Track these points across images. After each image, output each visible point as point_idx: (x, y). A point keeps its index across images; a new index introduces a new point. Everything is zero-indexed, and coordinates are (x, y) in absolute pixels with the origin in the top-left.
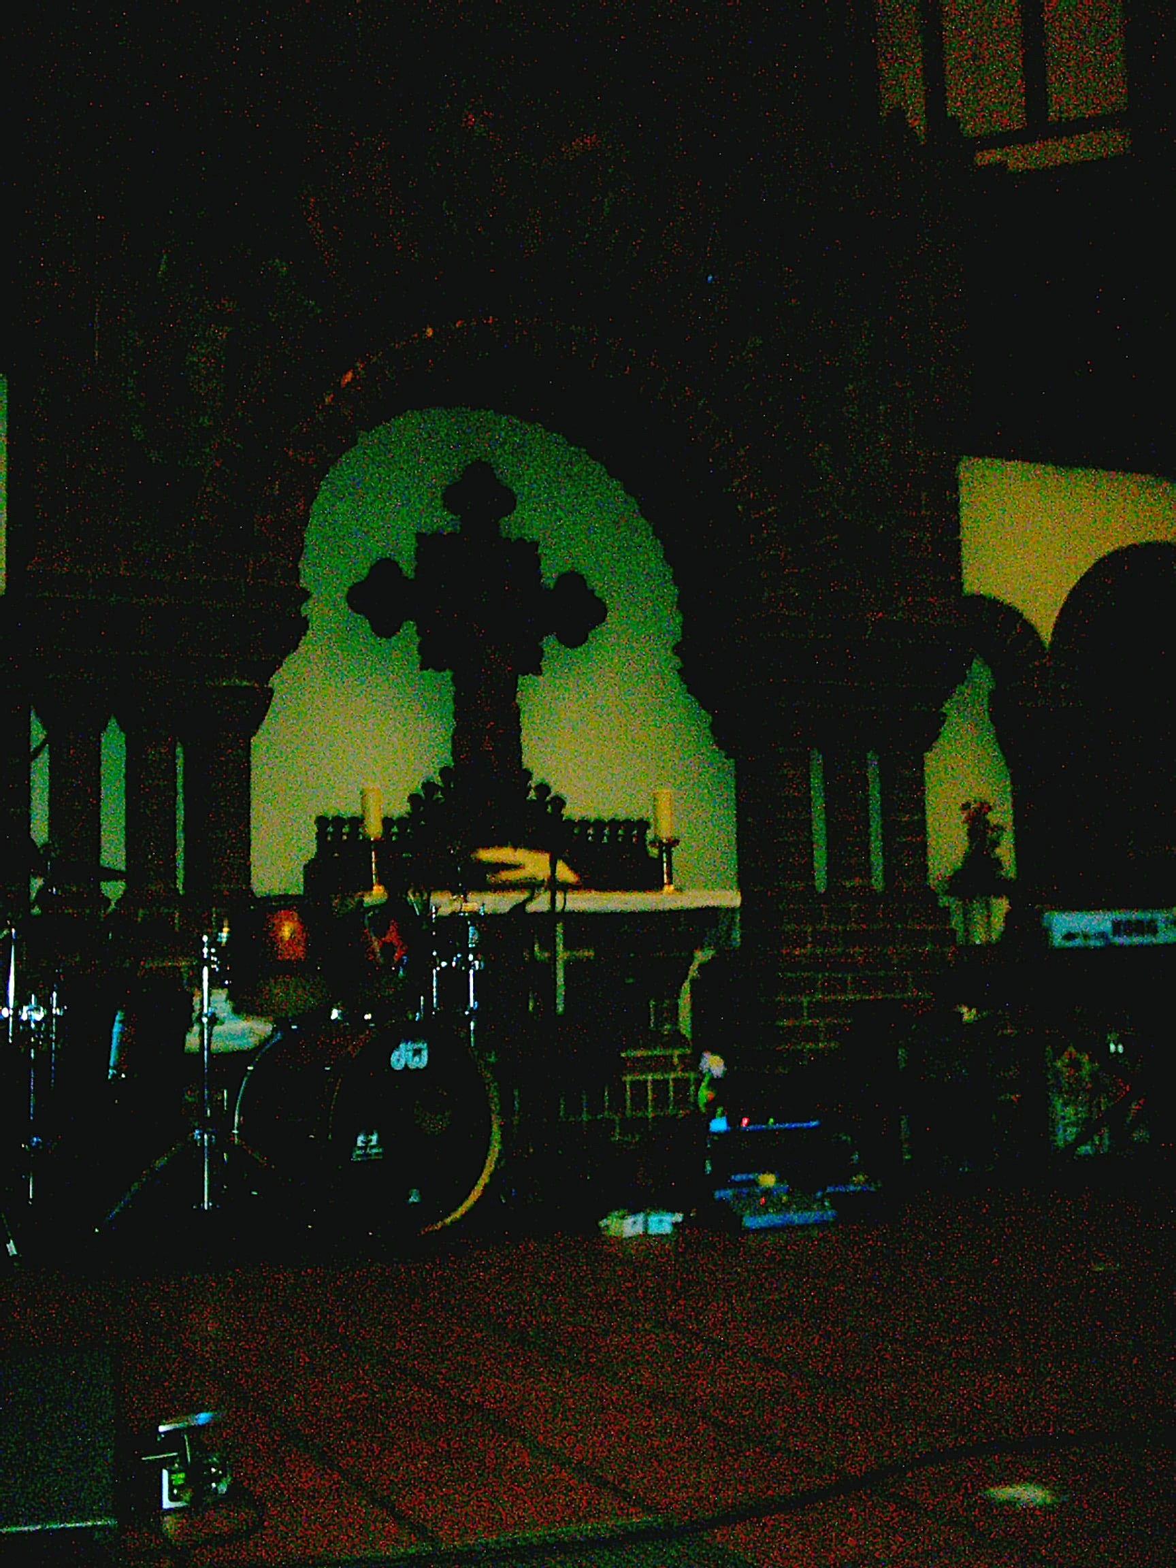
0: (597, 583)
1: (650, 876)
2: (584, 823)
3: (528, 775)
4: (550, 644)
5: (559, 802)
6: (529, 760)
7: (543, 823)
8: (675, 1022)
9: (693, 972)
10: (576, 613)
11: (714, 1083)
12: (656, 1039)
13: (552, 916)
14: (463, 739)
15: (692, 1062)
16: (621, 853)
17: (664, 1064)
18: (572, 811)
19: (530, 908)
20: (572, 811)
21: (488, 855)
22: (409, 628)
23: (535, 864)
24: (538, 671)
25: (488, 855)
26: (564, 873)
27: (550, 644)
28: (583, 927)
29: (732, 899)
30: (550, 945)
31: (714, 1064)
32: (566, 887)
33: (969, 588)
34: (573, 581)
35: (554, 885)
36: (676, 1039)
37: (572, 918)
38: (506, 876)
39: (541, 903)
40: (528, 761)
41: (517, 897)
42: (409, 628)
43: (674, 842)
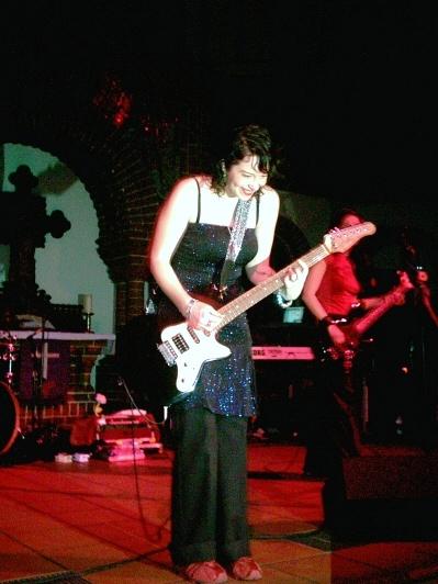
0: (68, 216)
1: (82, 327)
2: (57, 305)
3: (38, 286)
4: (48, 237)
5: (49, 297)
6: (38, 280)
7: (40, 304)
8: (89, 381)
9: (97, 363)
10: (59, 225)
11: (101, 406)
12: (81, 388)
13: (43, 341)
14: (11, 273)
15: (93, 397)
16: (73, 317)
17: (85, 397)
18: (53, 301)
19: (35, 337)
20: (53, 301)
21: (20, 317)
22: (49, 213)
23: (36, 322)
24: (43, 247)
25: (20, 317)
26: (49, 325)
27: (48, 237)
28: (55, 345)
29: (114, 337)
30: (41, 351)
31: (102, 399)
32: (49, 330)
33: (8, 247)
34: (58, 214)
35: (45, 330)
36: (89, 388)
37: (51, 342)
38: (26, 325)
39: (39, 336)
40: (37, 281)
41: (31, 333)
42: (49, 213)
43: (92, 314)
